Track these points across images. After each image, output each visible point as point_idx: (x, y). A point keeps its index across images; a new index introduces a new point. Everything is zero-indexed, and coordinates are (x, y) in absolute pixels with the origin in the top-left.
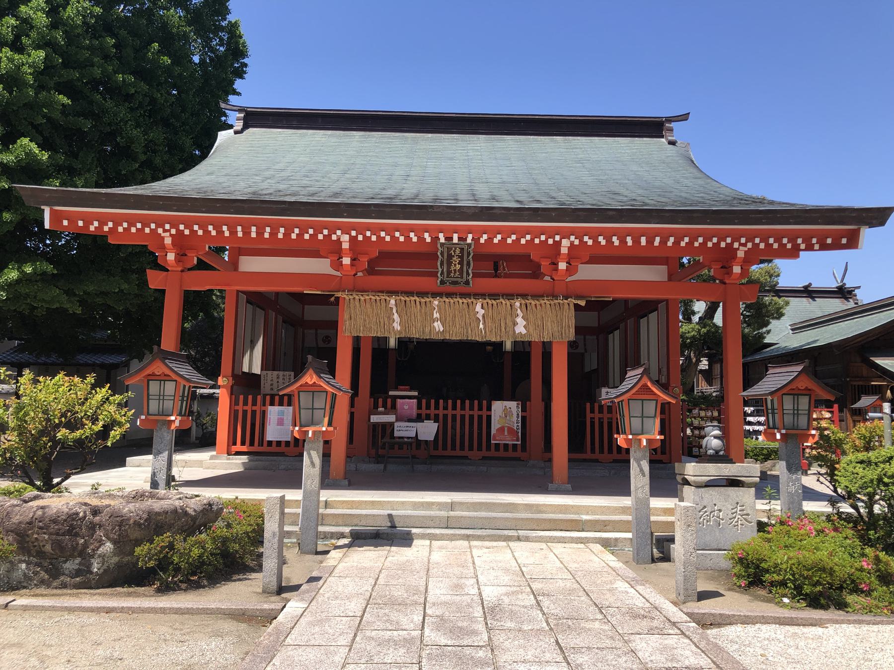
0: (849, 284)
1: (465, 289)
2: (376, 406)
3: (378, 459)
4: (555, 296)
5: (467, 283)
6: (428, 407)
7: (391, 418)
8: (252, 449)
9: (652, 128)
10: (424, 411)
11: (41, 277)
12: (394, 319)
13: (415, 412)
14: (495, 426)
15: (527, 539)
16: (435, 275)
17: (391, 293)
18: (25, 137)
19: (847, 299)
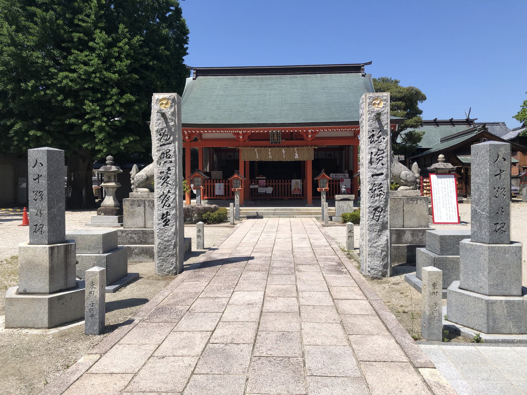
0: (471, 118)
1: (278, 144)
2: (252, 183)
3: (253, 200)
4: (308, 146)
5: (279, 143)
6: (269, 182)
7: (257, 186)
8: (210, 198)
9: (356, 69)
10: (268, 184)
11: (135, 141)
12: (257, 155)
13: (265, 184)
14: (293, 188)
15: (295, 217)
16: (269, 140)
17: (256, 147)
18: (127, 93)
19: (470, 125)
